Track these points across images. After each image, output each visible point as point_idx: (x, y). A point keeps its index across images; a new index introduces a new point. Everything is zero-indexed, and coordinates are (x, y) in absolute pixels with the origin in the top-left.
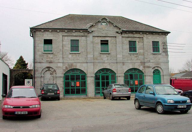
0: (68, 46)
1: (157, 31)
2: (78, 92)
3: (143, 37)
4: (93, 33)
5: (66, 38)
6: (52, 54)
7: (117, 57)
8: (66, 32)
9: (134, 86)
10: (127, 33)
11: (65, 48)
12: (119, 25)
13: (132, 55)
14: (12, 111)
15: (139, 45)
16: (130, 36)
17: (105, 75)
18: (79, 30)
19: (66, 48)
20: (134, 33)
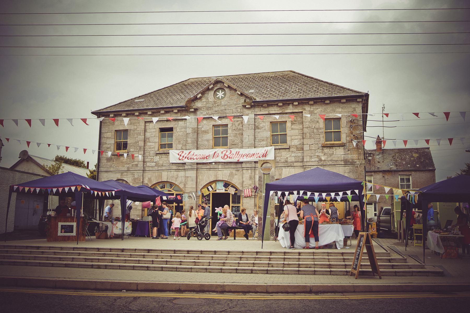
3: (302, 112)
11: (149, 144)
12: (251, 92)
14: (320, 185)
15: (292, 129)
19: (151, 144)
20: (342, 101)
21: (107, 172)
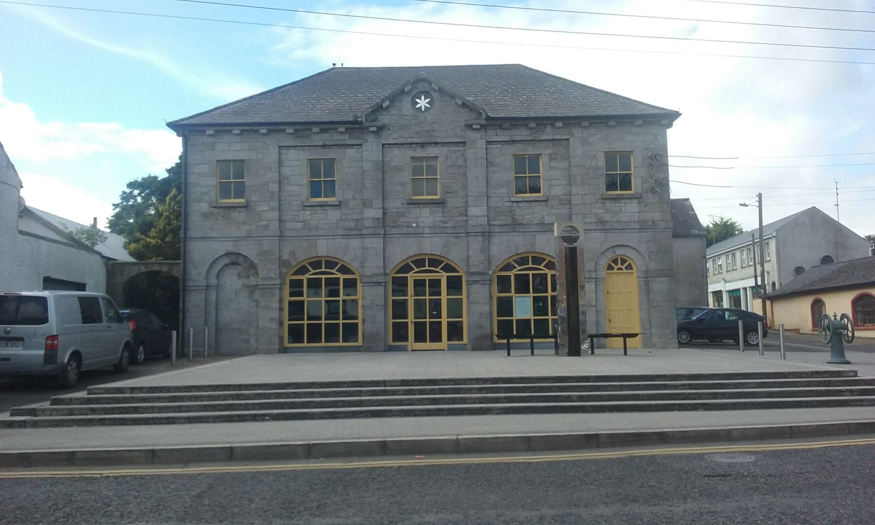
0: (506, 174)
1: (568, 115)
2: (332, 333)
3: (568, 139)
4: (384, 134)
5: (292, 154)
6: (243, 209)
7: (467, 216)
8: (264, 135)
9: (550, 317)
10: (504, 129)
11: (289, 188)
13: (524, 204)
16: (519, 138)
17: (427, 277)
18: (306, 127)
21: (203, 238)
